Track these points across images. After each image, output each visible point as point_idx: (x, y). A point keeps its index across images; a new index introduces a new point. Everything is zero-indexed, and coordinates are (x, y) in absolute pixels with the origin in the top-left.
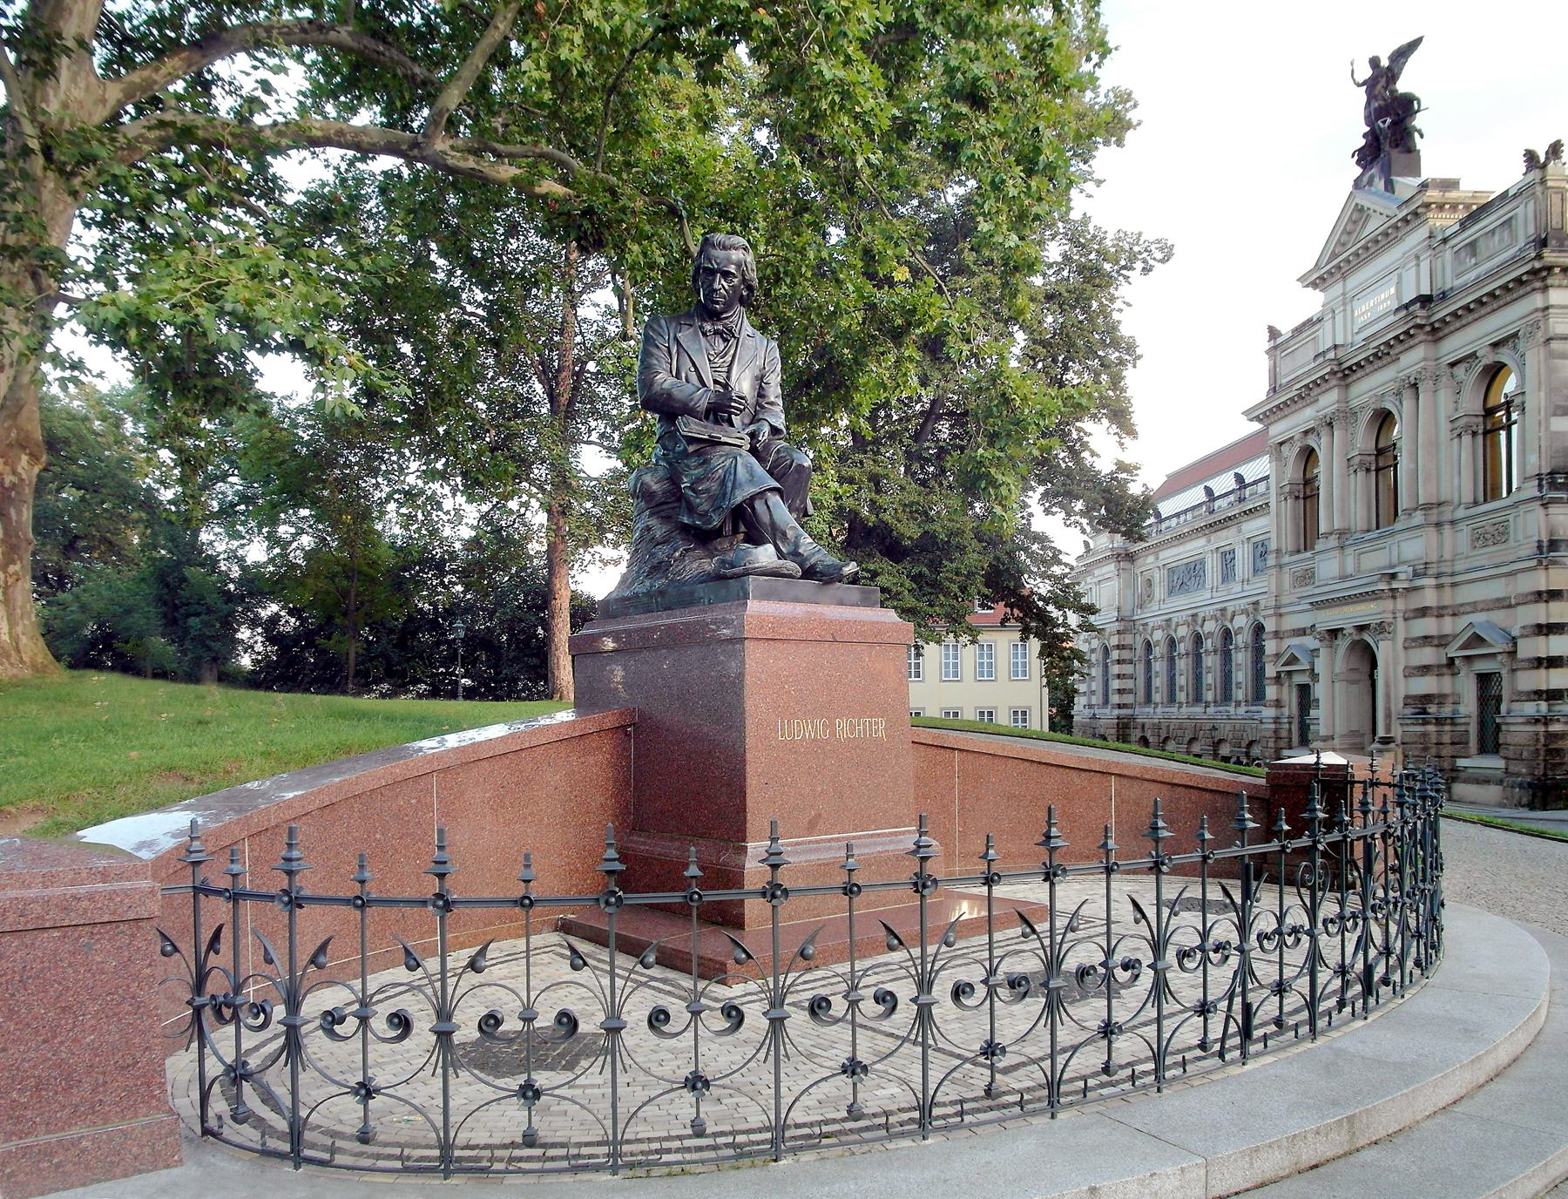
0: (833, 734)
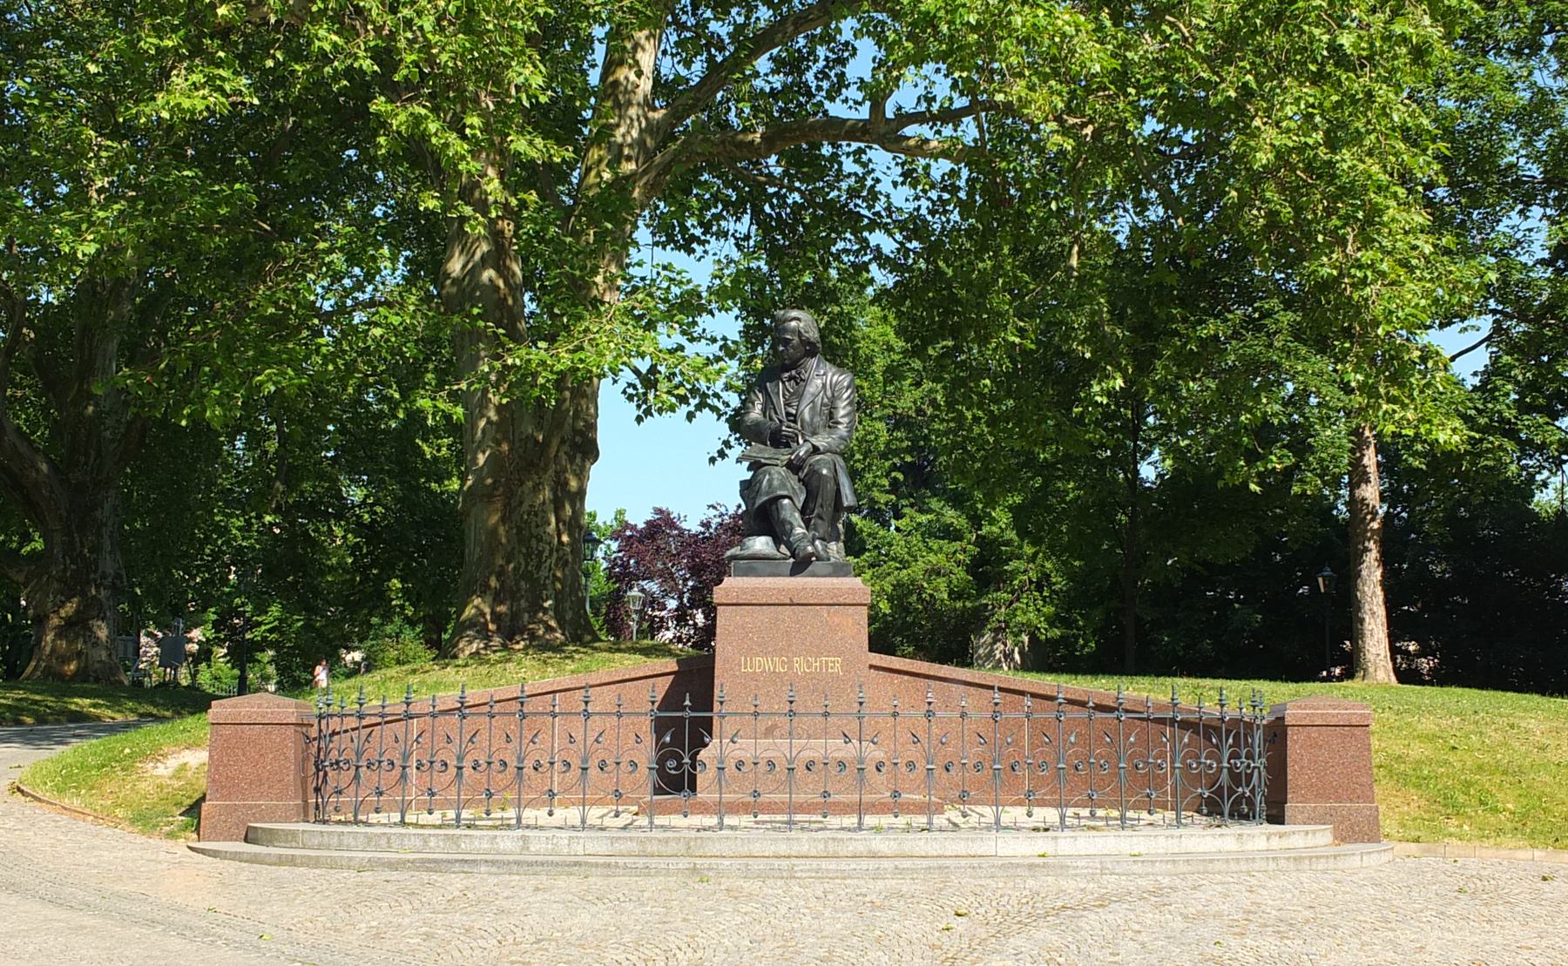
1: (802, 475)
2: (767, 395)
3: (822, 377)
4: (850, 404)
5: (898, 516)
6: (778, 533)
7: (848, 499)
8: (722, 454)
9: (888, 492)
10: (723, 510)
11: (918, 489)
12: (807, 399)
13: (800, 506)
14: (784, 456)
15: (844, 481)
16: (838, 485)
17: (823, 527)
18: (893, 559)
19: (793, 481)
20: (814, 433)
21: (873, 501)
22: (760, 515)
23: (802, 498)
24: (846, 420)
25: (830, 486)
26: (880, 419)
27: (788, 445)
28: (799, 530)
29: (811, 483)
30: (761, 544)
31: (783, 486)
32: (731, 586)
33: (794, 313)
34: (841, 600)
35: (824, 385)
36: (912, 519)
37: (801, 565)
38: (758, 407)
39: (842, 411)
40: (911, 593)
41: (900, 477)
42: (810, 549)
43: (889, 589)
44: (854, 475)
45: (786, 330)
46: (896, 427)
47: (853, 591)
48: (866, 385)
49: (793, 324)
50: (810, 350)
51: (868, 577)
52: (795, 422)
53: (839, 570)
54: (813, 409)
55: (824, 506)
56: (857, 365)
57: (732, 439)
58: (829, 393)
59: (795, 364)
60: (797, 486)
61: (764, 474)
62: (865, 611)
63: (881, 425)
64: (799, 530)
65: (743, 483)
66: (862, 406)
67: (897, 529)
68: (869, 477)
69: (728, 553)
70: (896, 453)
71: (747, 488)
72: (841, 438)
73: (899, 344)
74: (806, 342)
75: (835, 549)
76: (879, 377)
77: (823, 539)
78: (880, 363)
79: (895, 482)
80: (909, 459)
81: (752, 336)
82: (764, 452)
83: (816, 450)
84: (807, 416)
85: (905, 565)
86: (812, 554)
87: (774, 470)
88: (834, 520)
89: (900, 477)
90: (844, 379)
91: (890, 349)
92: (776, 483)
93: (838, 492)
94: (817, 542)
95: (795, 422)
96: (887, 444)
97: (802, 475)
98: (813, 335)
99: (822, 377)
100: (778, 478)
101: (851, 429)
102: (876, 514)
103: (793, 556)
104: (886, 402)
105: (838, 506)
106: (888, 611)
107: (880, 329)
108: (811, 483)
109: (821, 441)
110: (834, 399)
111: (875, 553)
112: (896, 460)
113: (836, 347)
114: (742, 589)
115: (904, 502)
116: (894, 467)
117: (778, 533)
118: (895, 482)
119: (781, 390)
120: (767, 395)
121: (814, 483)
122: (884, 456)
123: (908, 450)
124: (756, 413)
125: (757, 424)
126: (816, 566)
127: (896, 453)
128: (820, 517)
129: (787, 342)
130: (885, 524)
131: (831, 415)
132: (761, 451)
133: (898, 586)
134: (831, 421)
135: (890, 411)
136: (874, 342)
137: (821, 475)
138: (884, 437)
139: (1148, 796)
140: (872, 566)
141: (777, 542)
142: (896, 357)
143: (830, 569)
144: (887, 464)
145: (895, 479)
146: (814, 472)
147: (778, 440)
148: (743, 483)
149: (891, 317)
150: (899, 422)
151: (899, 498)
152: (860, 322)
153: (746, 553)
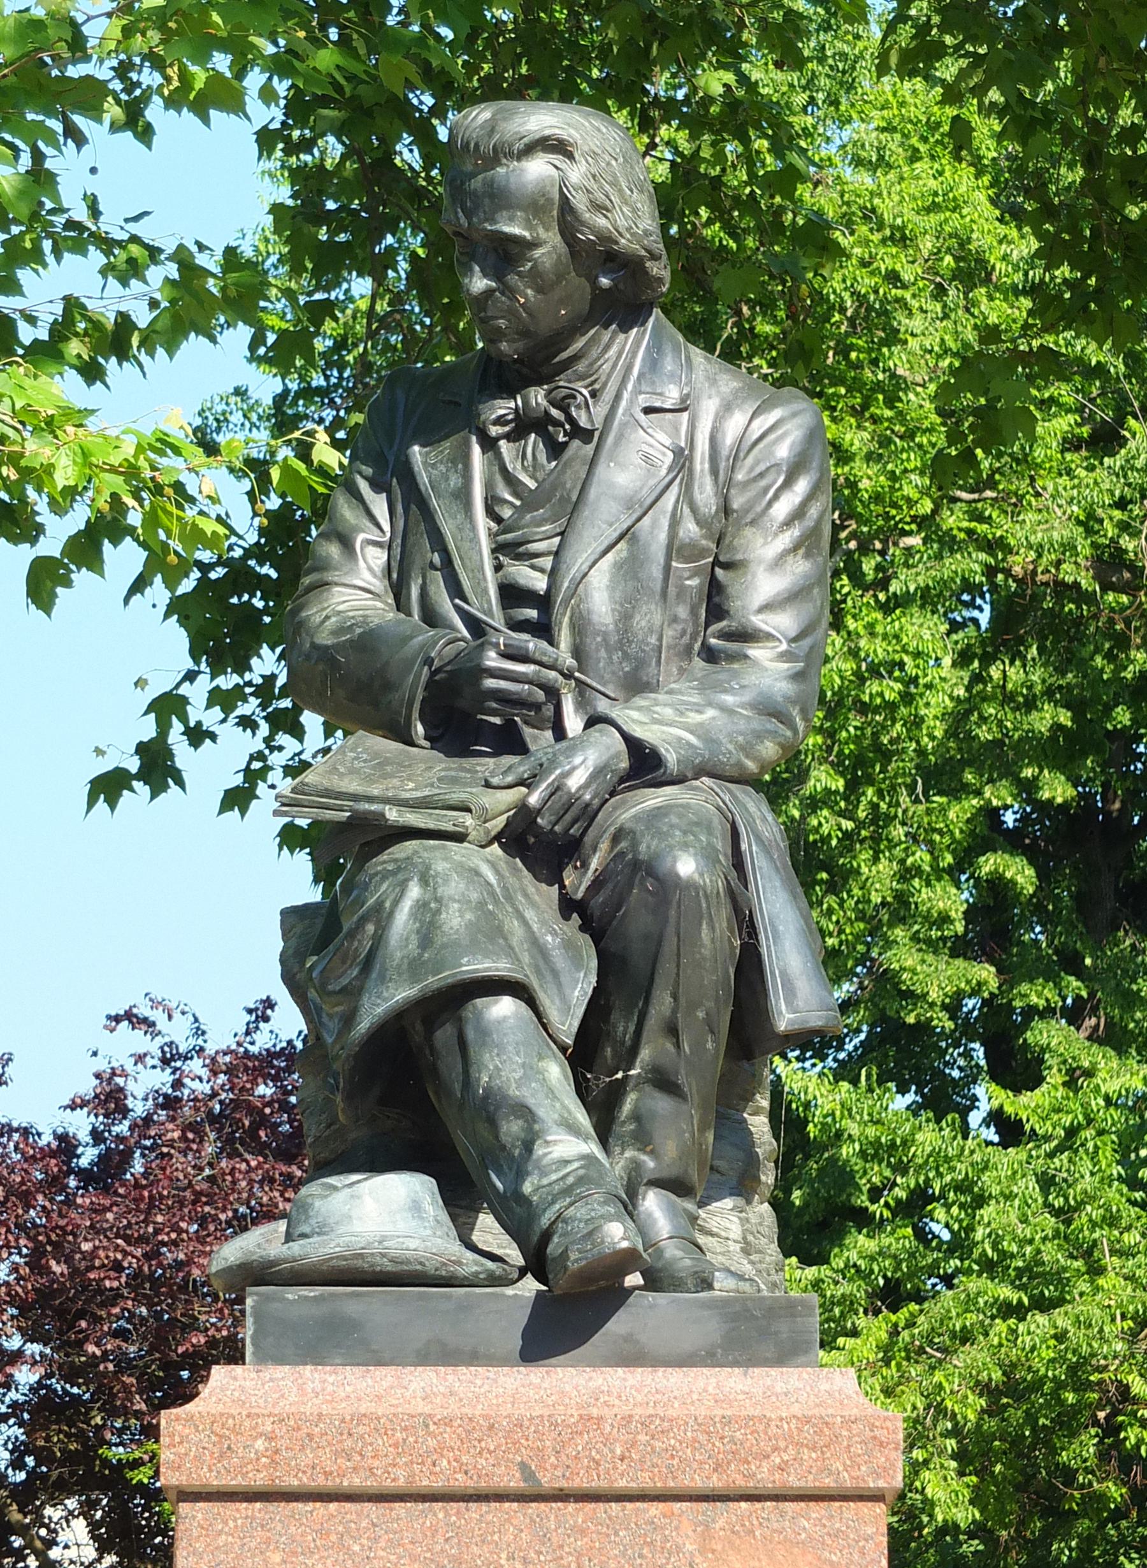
1: (577, 882)
2: (413, 503)
3: (674, 420)
4: (805, 545)
5: (1018, 1069)
6: (464, 1158)
7: (799, 993)
8: (156, 766)
9: (960, 948)
10: (179, 1032)
11: (1101, 932)
12: (601, 521)
13: (567, 1026)
14: (491, 790)
15: (777, 905)
16: (746, 923)
17: (676, 1130)
18: (989, 1267)
19: (535, 907)
20: (636, 685)
21: (887, 987)
22: (388, 1083)
23: (581, 987)
24: (784, 622)
25: (714, 937)
26: (927, 598)
27: (510, 742)
28: (566, 1144)
29: (621, 922)
30: (384, 1211)
31: (489, 931)
32: (241, 1413)
33: (541, 119)
34: (765, 1476)
35: (682, 459)
36: (1074, 1077)
37: (573, 1309)
38: (371, 562)
39: (771, 577)
40: (1069, 1423)
41: (1021, 874)
42: (617, 1234)
43: (970, 1408)
44: (816, 867)
45: (500, 199)
46: (1004, 639)
47: (820, 1431)
48: (857, 439)
49: (538, 169)
50: (617, 292)
51: (865, 1348)
52: (544, 630)
53: (752, 1335)
54: (630, 569)
55: (681, 1027)
56: (810, 355)
57: (197, 692)
58: (706, 495)
59: (540, 359)
60: (558, 935)
61: (400, 875)
62: (875, 1522)
63: (922, 629)
64: (566, 1144)
65: (293, 917)
66: (852, 546)
67: (1010, 1131)
68: (878, 877)
69: (233, 1251)
70: (999, 759)
71: (319, 944)
72: (770, 710)
73: (1012, 249)
74: (596, 255)
75: (736, 1233)
76: (920, 403)
77: (677, 1186)
78: (926, 340)
79: (994, 899)
80: (1057, 789)
81: (324, 227)
82: (393, 774)
83: (643, 765)
84: (600, 597)
85: (1042, 1291)
86: (627, 1260)
87: (442, 858)
88: (725, 1114)
89: (1021, 874)
90: (783, 427)
91: (973, 271)
92: (454, 920)
93: (749, 969)
94: (652, 1202)
95: (544, 630)
96: (959, 719)
97: (577, 882)
98: (633, 222)
99: (674, 420)
100: (461, 901)
101: (807, 661)
102: (898, 1048)
103: (537, 1263)
104: (953, 520)
105: (748, 1030)
106: (965, 1515)
107: (925, 177)
108: (621, 922)
109: (669, 720)
110: (726, 522)
111: (901, 1239)
112: (999, 794)
113: (740, 275)
114: (350, 1425)
115: (1036, 994)
116: (988, 831)
117: (464, 1158)
118: (994, 899)
119: (471, 481)
120: (413, 503)
121: (637, 920)
122: (941, 777)
123: (1060, 751)
124: (355, 590)
125: (365, 642)
126: (643, 1314)
127: (999, 759)
128: (663, 1081)
129: (505, 255)
130: (944, 1101)
131: (715, 602)
132: (382, 767)
133: (1007, 1389)
134: (716, 627)
135: (973, 564)
136: (901, 238)
137: (666, 887)
138: (945, 686)
139: (1081, 1294)
140: (892, 1295)
141: (461, 1197)
142: (995, 310)
143: (711, 1330)
144: (958, 813)
145: (997, 887)
146: (635, 870)
147: (464, 716)
148: (293, 917)
149: (985, 132)
150: (1024, 615)
151: (1009, 974)
152: (831, 143)
153: (312, 1250)
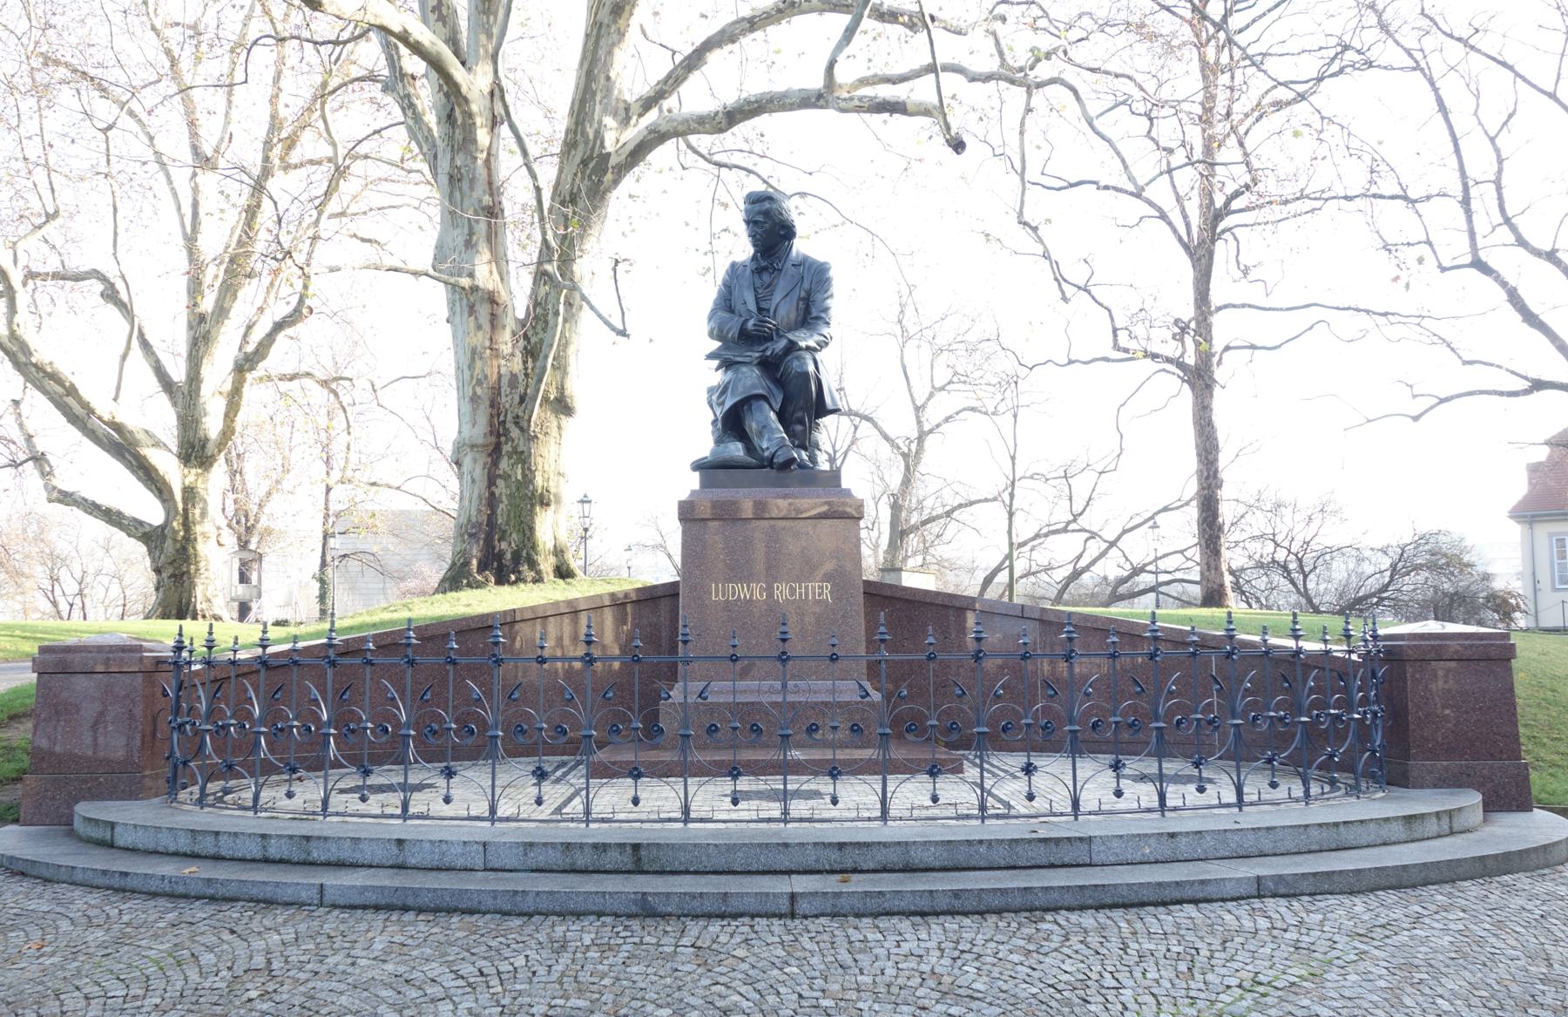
0: (770, 595)
13: (777, 407)
23: (780, 398)
